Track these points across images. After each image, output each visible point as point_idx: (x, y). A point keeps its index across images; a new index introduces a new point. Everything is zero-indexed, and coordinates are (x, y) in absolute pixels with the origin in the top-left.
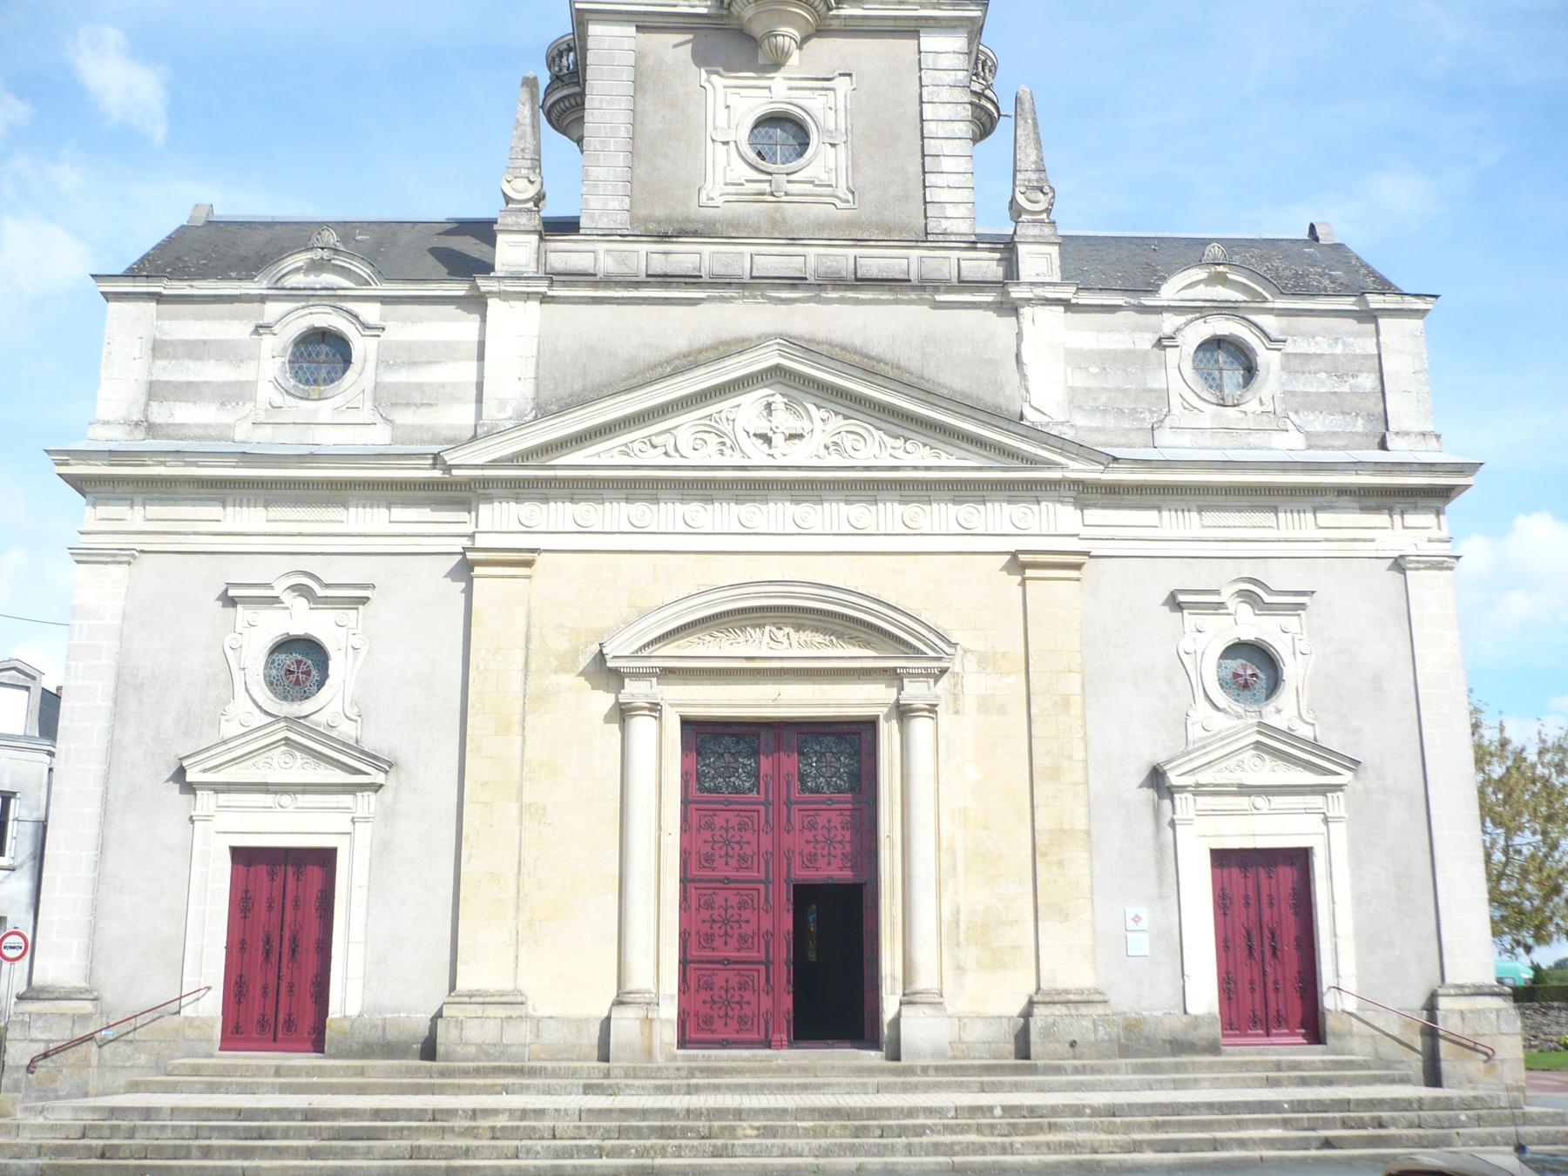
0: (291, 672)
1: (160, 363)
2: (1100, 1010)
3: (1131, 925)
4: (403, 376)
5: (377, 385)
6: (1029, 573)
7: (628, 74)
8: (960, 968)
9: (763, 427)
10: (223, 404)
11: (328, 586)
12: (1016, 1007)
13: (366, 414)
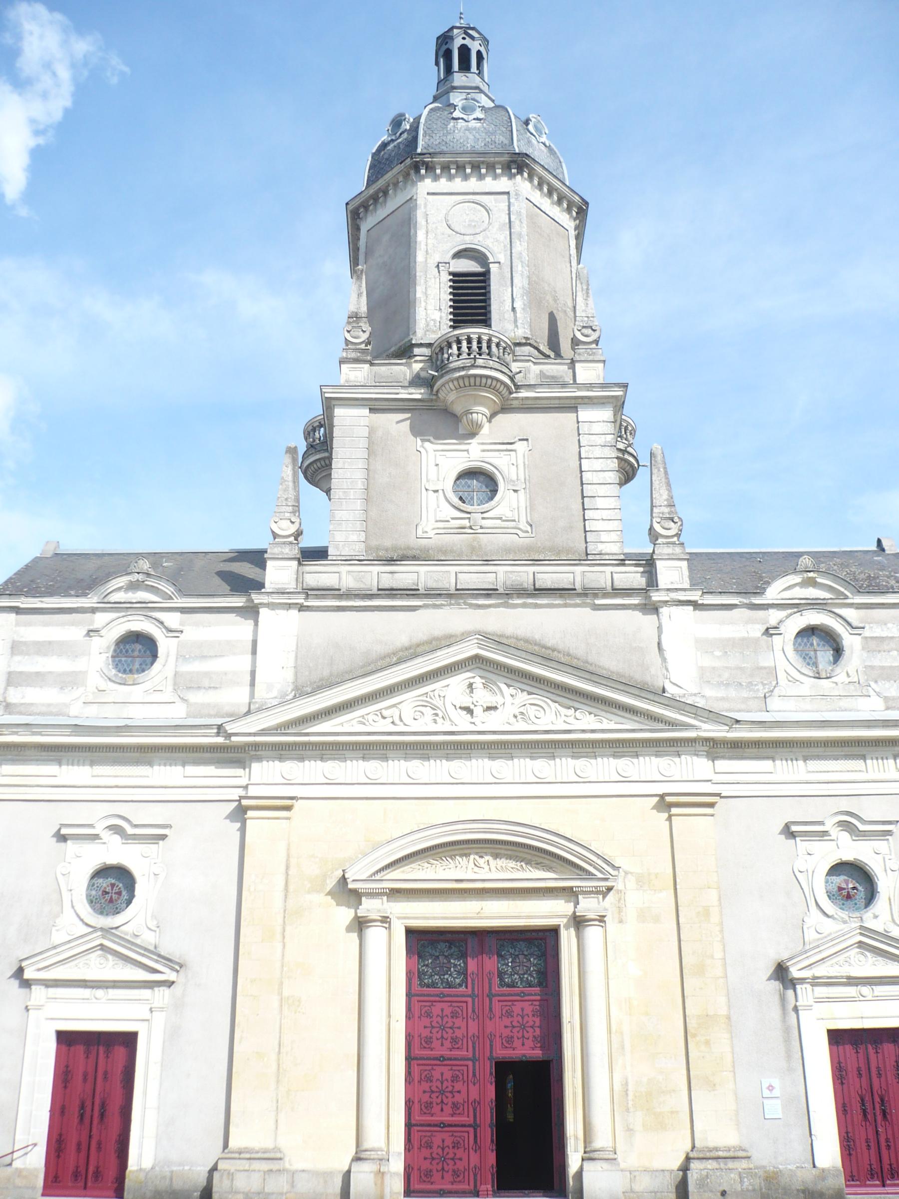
0: (107, 893)
1: (17, 658)
2: (744, 1164)
3: (766, 1093)
4: (196, 667)
5: (176, 674)
6: (674, 811)
7: (364, 443)
8: (629, 1130)
9: (467, 702)
10: (62, 688)
11: (136, 826)
12: (677, 1162)
13: (168, 695)
